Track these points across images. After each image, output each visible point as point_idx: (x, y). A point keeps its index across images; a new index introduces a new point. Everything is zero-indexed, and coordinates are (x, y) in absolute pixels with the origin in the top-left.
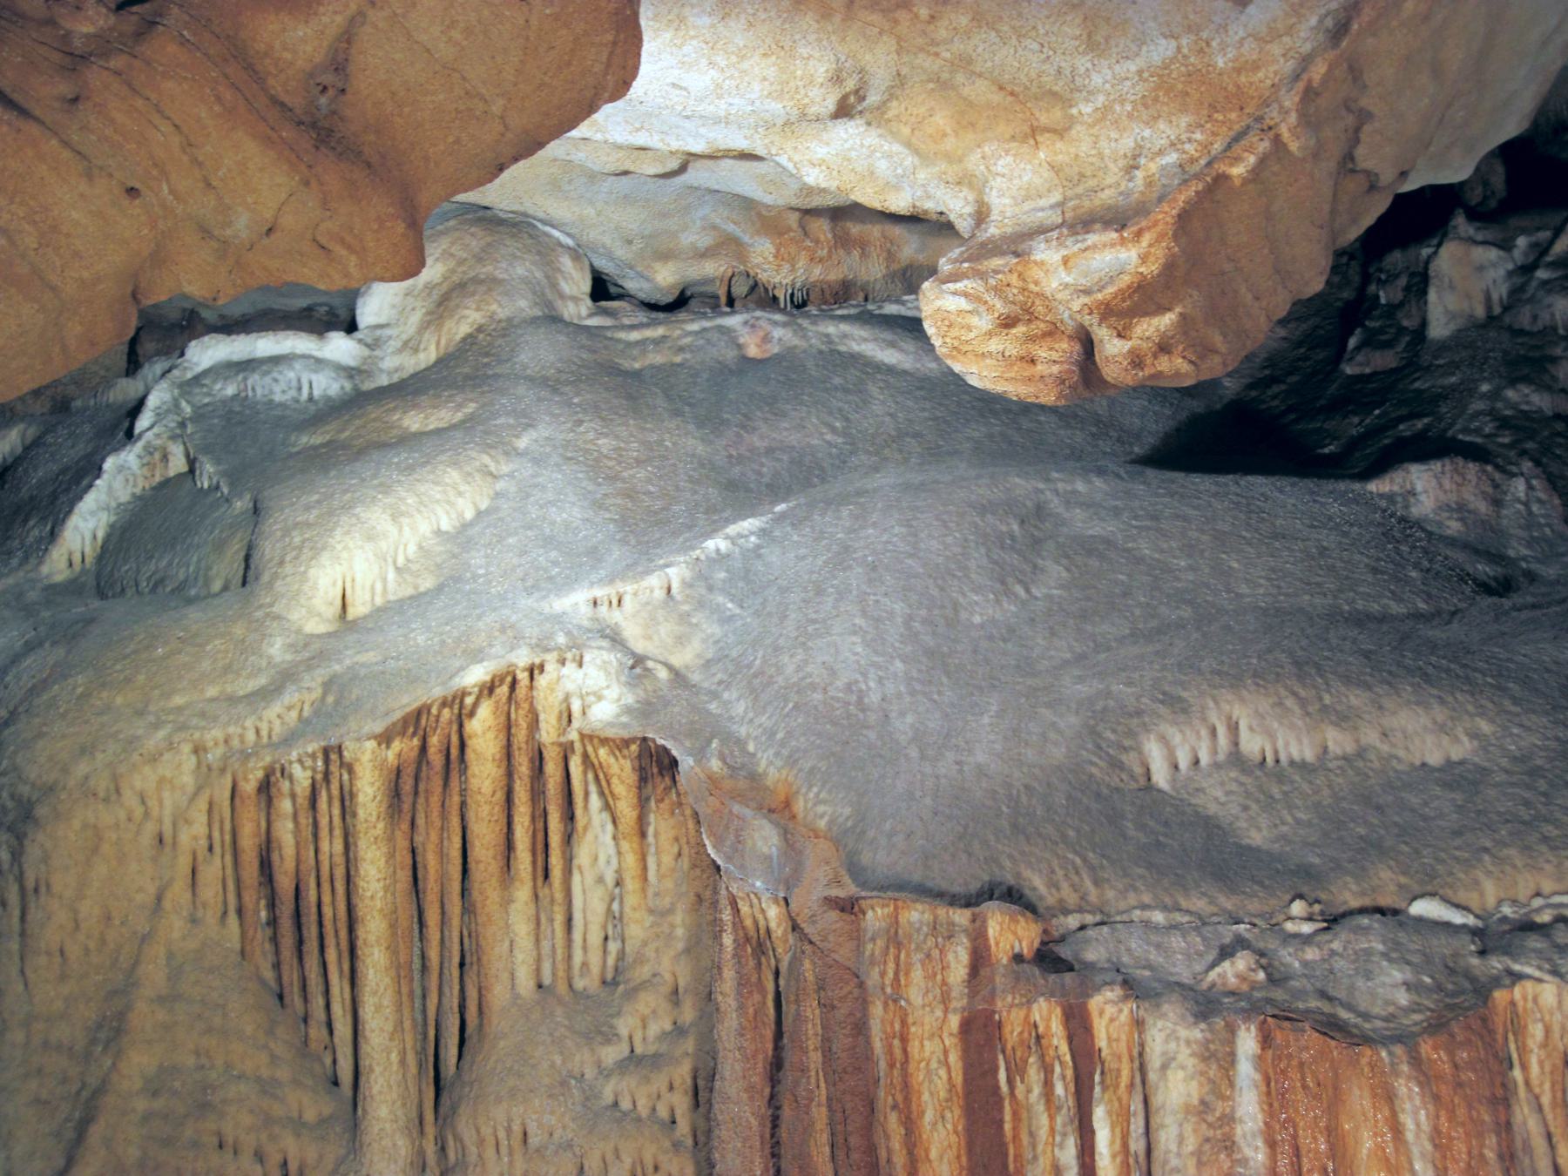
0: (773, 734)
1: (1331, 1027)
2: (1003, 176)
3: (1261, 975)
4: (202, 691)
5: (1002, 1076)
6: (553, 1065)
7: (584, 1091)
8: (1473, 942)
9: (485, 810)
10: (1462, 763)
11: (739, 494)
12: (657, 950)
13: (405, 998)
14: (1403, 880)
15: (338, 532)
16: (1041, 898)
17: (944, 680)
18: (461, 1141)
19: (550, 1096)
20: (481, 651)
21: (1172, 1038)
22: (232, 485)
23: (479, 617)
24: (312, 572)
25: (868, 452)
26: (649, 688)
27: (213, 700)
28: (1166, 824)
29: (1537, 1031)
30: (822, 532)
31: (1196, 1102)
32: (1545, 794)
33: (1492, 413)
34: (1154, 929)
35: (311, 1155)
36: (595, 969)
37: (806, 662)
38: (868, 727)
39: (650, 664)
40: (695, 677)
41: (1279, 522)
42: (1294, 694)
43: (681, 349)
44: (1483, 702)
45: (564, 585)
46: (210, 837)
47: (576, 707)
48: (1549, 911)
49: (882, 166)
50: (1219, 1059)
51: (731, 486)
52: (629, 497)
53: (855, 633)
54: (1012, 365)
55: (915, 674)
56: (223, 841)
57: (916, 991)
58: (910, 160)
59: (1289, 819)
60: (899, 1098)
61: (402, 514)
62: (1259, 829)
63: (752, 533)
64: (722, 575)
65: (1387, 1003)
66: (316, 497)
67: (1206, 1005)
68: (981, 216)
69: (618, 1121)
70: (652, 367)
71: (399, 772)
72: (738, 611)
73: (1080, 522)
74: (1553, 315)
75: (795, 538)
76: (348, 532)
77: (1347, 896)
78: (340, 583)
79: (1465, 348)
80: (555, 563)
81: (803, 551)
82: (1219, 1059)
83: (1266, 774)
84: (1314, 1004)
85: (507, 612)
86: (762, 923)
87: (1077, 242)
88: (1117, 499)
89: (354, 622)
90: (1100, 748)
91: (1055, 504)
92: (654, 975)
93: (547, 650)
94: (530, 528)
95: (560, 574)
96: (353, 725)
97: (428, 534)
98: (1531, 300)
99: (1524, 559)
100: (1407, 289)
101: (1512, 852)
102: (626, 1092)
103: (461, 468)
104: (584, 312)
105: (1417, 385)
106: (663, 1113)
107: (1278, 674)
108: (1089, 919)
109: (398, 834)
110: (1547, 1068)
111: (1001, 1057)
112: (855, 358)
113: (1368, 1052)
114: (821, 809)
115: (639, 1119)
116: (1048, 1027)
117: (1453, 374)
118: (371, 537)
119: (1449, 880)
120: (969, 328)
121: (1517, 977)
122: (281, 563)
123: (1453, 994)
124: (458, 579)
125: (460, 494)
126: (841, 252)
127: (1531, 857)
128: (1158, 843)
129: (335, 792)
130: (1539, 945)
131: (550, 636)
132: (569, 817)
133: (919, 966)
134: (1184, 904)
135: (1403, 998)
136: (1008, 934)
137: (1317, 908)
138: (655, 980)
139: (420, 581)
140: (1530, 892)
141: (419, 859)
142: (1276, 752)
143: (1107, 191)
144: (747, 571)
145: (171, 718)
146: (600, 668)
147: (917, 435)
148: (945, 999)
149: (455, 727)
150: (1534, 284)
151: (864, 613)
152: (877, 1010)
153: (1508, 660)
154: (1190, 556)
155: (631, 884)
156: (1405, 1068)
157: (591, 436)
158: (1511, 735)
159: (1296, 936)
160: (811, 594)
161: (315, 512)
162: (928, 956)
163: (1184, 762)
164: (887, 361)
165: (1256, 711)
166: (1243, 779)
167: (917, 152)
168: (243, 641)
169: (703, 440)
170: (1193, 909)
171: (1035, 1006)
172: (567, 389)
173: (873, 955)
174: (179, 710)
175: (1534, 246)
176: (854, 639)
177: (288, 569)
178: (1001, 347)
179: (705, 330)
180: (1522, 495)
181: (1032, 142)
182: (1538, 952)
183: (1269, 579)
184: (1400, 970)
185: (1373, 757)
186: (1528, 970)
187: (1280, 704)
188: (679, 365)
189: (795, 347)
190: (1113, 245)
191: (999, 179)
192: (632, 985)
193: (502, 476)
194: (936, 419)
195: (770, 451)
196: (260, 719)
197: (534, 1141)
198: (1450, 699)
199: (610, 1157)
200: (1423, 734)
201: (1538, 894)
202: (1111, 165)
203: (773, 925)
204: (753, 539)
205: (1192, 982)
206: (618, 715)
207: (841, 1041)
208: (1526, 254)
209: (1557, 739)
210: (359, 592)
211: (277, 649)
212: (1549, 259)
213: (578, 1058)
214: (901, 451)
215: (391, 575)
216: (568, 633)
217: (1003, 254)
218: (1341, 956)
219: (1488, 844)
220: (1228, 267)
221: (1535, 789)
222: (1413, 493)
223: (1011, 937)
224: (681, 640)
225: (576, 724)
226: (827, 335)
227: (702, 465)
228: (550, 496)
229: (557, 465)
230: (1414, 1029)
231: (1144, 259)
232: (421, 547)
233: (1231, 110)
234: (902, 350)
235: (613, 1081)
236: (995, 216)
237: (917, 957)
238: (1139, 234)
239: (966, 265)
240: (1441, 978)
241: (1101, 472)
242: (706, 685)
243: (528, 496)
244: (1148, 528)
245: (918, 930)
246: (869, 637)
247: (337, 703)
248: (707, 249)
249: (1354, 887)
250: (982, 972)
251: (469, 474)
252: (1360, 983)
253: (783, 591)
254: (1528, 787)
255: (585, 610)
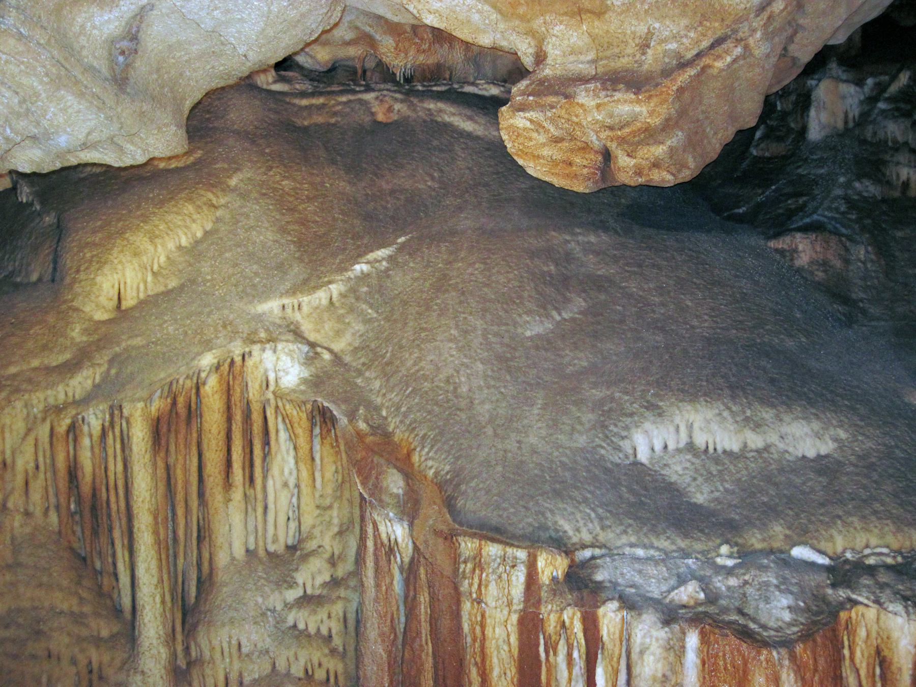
0: (398, 408)
1: (745, 634)
2: (557, 37)
3: (702, 596)
4: (29, 362)
5: (542, 649)
6: (256, 604)
7: (275, 618)
8: (829, 579)
9: (214, 430)
10: (827, 456)
11: (373, 225)
12: (321, 532)
13: (164, 562)
14: (788, 532)
15: (115, 251)
16: (569, 538)
17: (508, 378)
18: (200, 646)
19: (255, 623)
20: (210, 341)
21: (648, 633)
22: (42, 203)
23: (210, 314)
24: (99, 279)
25: (455, 196)
26: (318, 366)
27: (35, 369)
28: (646, 489)
29: (862, 633)
30: (428, 261)
31: (660, 675)
32: (875, 482)
33: (847, 199)
34: (637, 560)
35: (106, 658)
36: (282, 540)
37: (420, 359)
38: (460, 410)
39: (319, 350)
40: (347, 359)
41: (716, 271)
42: (729, 408)
43: (335, 114)
44: (842, 418)
45: (265, 294)
46: (37, 460)
47: (272, 377)
48: (873, 557)
49: (476, 17)
50: (676, 650)
51: (368, 217)
52: (303, 224)
53: (450, 340)
54: (557, 165)
55: (490, 373)
56: (45, 463)
57: (492, 592)
58: (494, 16)
59: (721, 489)
60: (478, 659)
61: (157, 237)
62: (702, 493)
63: (383, 259)
64: (365, 289)
65: (777, 620)
66: (99, 223)
67: (670, 615)
68: (540, 58)
69: (297, 637)
70: (316, 125)
71: (158, 419)
72: (375, 315)
73: (592, 265)
74: (886, 133)
75: (412, 265)
76: (122, 251)
77: (754, 541)
78: (116, 286)
79: (831, 149)
80: (256, 274)
81: (417, 275)
82: (676, 650)
83: (708, 458)
84: (734, 617)
85: (226, 312)
86: (392, 538)
87: (607, 96)
88: (616, 249)
89: (126, 310)
90: (607, 437)
91: (577, 250)
92: (320, 547)
93: (254, 342)
94: (239, 246)
95: (260, 282)
96: (130, 394)
97: (174, 249)
98: (874, 122)
99: (861, 300)
100: (796, 104)
101: (855, 519)
102: (301, 619)
103: (194, 203)
104: (270, 80)
105: (799, 171)
106: (324, 631)
107: (719, 395)
108: (597, 552)
109: (158, 459)
110: (866, 654)
111: (541, 637)
112: (446, 126)
113: (765, 652)
114: (430, 463)
115: (309, 636)
116: (572, 623)
117: (822, 167)
118: (136, 254)
119: (816, 534)
120: (531, 139)
121: (855, 603)
122: (78, 271)
123: (817, 614)
124: (193, 282)
125: (194, 221)
126: (437, 46)
127: (866, 523)
128: (642, 503)
129: (118, 434)
130: (868, 582)
131: (255, 332)
132: (266, 443)
133: (494, 583)
134: (656, 544)
135: (787, 616)
136: (551, 566)
137: (735, 549)
138: (320, 550)
139: (168, 281)
140: (863, 544)
141: (172, 473)
142: (715, 443)
143: (626, 58)
144: (381, 286)
145: (9, 383)
146: (287, 354)
147: (487, 185)
148: (510, 604)
149: (194, 391)
150: (876, 111)
151: (457, 326)
152: (467, 606)
153: (858, 387)
154: (661, 295)
155: (305, 490)
156: (786, 662)
157: (278, 178)
158: (857, 440)
159: (724, 567)
160: (423, 309)
161: (100, 235)
162: (500, 577)
163: (658, 447)
164: (466, 129)
165: (705, 418)
166: (694, 460)
167: (500, 12)
168: (54, 327)
169: (349, 183)
170: (661, 547)
171: (565, 612)
172: (261, 141)
173: (464, 571)
174: (14, 376)
175: (877, 85)
176: (451, 345)
177: (82, 276)
178: (550, 153)
179: (350, 101)
180: (862, 257)
181: (579, 18)
182: (868, 586)
183: (711, 316)
184: (786, 598)
185: (774, 452)
186: (860, 599)
187: (720, 414)
188: (334, 125)
189: (409, 117)
190: (631, 102)
191: (554, 39)
192: (305, 552)
193: (220, 207)
194: (498, 173)
195: (392, 192)
196: (68, 385)
197: (245, 650)
198: (823, 416)
199: (292, 659)
200: (804, 438)
201: (867, 546)
202: (630, 41)
203: (400, 540)
204: (384, 263)
205: (660, 597)
206: (299, 385)
207: (445, 623)
208: (872, 90)
209: (885, 445)
210: (128, 289)
211: (76, 333)
212: (886, 95)
213: (272, 598)
214: (476, 196)
215: (150, 278)
216: (267, 330)
217: (557, 94)
218: (751, 585)
219: (841, 513)
220: (701, 117)
221: (870, 478)
222: (795, 251)
223: (551, 568)
224: (338, 333)
225: (271, 388)
226: (429, 110)
227: (349, 201)
228: (252, 222)
229: (255, 199)
230: (792, 637)
231: (651, 113)
232: (168, 258)
233: (716, 21)
234: (476, 122)
235: (294, 611)
236: (549, 61)
237: (493, 577)
238: (650, 97)
239: (531, 98)
240: (809, 602)
241: (606, 229)
242: (354, 364)
243: (238, 222)
244: (635, 273)
245: (495, 560)
246: (460, 344)
247: (117, 374)
248: (351, 40)
249: (759, 536)
250: (533, 588)
251: (199, 207)
252: (762, 605)
253: (405, 303)
254: (867, 476)
255: (277, 311)
